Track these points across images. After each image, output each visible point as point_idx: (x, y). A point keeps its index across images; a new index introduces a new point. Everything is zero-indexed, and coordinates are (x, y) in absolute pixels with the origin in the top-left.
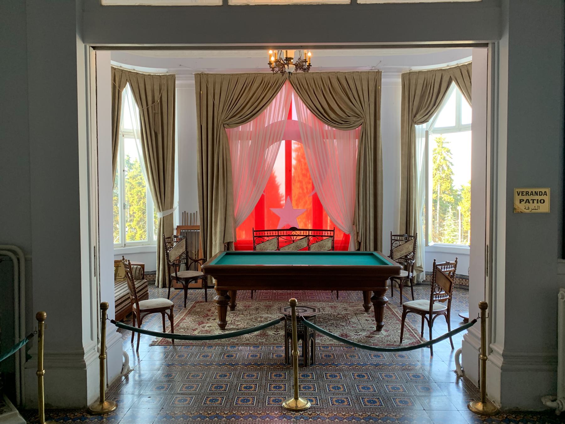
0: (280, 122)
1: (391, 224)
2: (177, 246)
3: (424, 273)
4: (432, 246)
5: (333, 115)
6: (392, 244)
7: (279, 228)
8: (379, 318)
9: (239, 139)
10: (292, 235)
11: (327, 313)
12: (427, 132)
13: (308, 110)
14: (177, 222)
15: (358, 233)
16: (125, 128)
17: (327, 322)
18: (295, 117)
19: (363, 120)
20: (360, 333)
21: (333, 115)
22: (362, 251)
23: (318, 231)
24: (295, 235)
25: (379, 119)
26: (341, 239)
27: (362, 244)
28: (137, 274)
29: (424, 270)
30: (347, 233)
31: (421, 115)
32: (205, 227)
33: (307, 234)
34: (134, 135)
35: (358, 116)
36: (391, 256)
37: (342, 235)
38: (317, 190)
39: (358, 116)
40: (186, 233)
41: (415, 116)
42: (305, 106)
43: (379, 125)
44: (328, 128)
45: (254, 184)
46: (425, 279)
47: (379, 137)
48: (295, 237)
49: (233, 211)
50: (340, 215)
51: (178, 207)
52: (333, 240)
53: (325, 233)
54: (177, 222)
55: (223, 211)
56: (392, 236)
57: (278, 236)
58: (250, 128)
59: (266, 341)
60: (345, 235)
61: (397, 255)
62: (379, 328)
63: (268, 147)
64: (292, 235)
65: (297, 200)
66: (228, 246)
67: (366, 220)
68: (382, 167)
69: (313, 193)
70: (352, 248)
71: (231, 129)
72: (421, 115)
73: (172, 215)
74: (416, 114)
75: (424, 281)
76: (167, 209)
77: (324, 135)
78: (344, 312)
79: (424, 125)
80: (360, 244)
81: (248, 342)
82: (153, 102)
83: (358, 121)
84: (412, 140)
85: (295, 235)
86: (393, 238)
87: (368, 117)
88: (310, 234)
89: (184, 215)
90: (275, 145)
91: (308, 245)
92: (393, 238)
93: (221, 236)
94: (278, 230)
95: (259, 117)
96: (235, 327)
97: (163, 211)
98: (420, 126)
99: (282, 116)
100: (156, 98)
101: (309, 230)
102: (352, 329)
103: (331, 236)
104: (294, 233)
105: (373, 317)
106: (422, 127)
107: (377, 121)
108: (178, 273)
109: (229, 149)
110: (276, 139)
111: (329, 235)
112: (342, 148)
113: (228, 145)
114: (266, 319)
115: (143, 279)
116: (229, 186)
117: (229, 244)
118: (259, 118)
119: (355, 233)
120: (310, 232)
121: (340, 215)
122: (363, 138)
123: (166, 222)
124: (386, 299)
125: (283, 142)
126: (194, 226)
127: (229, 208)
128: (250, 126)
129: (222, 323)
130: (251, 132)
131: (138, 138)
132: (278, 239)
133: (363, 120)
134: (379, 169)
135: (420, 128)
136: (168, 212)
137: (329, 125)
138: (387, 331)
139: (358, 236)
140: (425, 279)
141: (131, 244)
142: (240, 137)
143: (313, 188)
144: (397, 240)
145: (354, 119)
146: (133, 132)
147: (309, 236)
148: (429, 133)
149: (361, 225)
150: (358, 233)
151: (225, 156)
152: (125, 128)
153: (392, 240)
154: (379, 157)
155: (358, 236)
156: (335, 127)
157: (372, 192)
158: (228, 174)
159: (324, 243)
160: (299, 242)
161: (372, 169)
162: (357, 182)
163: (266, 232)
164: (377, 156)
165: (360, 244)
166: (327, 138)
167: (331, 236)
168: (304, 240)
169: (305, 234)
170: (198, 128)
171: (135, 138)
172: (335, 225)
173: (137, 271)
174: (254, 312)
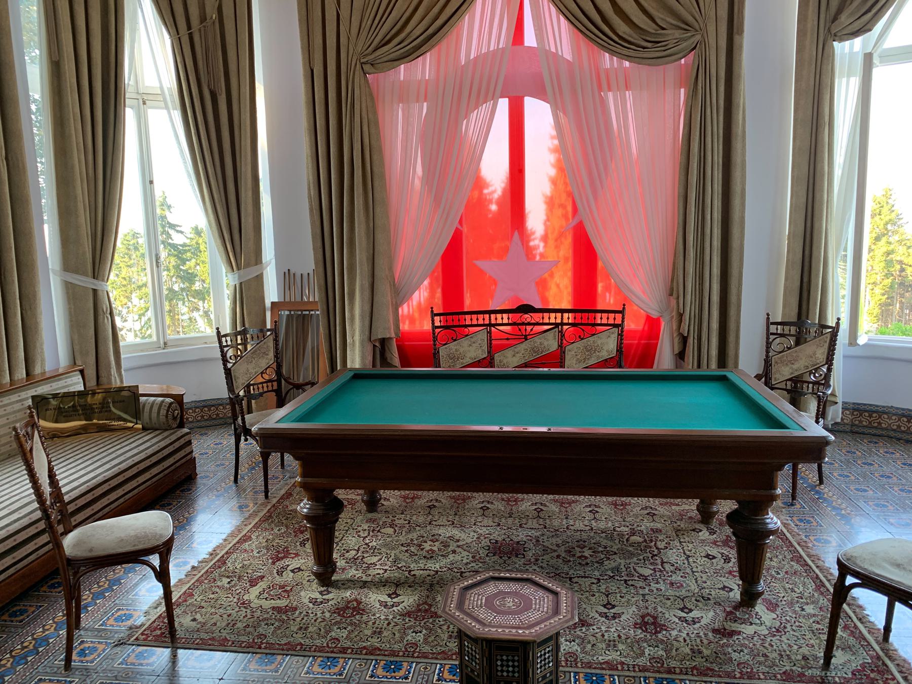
0: (495, 52)
1: (761, 295)
2: (254, 351)
3: (840, 405)
4: (865, 345)
5: (623, 28)
6: (768, 345)
7: (492, 307)
8: (750, 569)
9: (401, 100)
10: (523, 324)
11: (602, 525)
12: (868, 59)
13: (562, 18)
14: (272, 293)
15: (681, 316)
16: (146, 84)
17: (601, 562)
18: (530, 39)
19: (698, 37)
20: (695, 614)
21: (623, 28)
22: (689, 368)
23: (585, 315)
24: (529, 324)
25: (741, 31)
26: (640, 328)
27: (690, 340)
28: (162, 418)
29: (840, 400)
30: (655, 314)
31: (852, 14)
32: (331, 305)
33: (559, 321)
34: (165, 100)
35: (686, 26)
36: (765, 376)
37: (643, 321)
38: (583, 214)
39: (686, 26)
40: (296, 318)
41: (835, 19)
42: (553, 9)
43: (741, 46)
44: (611, 60)
45: (437, 200)
46: (839, 420)
47: (739, 76)
48: (529, 328)
49: (391, 269)
50: (637, 278)
51: (274, 261)
52: (620, 335)
53: (599, 318)
54: (272, 293)
55: (366, 268)
56: (769, 323)
57: (490, 325)
58: (423, 72)
59: (426, 640)
60: (649, 318)
61: (782, 373)
62: (750, 597)
63: (467, 116)
64: (523, 324)
65: (556, 240)
66: (380, 348)
67: (702, 284)
68: (744, 155)
69: (575, 222)
70: (665, 359)
71: (381, 75)
72: (852, 14)
73: (259, 279)
74: (839, 11)
75: (836, 423)
76: (247, 265)
77: (603, 82)
78: (646, 525)
79: (857, 43)
80: (684, 340)
81: (375, 642)
82: (203, 18)
83: (685, 40)
84: (826, 80)
85: (529, 324)
86: (773, 329)
87: (711, 28)
88: (565, 321)
89: (287, 278)
90: (485, 108)
91: (561, 346)
92: (773, 329)
93: (363, 326)
94: (490, 312)
95: (444, 43)
96: (359, 574)
97: (239, 269)
98: (847, 43)
99: (500, 38)
100: (208, 10)
101: (562, 311)
102: (670, 592)
103: (615, 326)
104: (527, 317)
105: (726, 543)
106: (852, 47)
107: (736, 38)
108: (247, 417)
109: (377, 123)
110: (488, 95)
111: (611, 321)
112: (645, 113)
113: (375, 113)
114: (446, 546)
115: (181, 425)
116: (378, 210)
117: (384, 342)
118: (445, 45)
119: (674, 313)
120: (566, 315)
121: (637, 278)
122: (697, 83)
123: (248, 294)
124: (773, 520)
125: (503, 105)
126: (309, 302)
127: (380, 262)
128: (424, 68)
129: (321, 570)
130: (427, 81)
131: (174, 109)
132: (489, 333)
133: (698, 37)
134: (737, 158)
135: (847, 50)
136: (252, 272)
137: (613, 53)
138: (772, 607)
139: (680, 321)
140: (839, 420)
141: (179, 343)
142: (403, 95)
143: (575, 210)
144: (782, 335)
145: (678, 34)
146: (163, 93)
147: (562, 324)
148: (876, 60)
149: (688, 297)
150: (681, 316)
151: (366, 141)
152: (146, 84)
153: (768, 334)
154: (737, 130)
155: (680, 321)
156: (628, 57)
157: (717, 215)
158: (376, 184)
159: (599, 342)
160: (538, 340)
161: (719, 159)
162: (682, 191)
163: (468, 317)
164: (734, 126)
165: (684, 340)
166: (610, 89)
167: (615, 326)
168: (550, 335)
169: (552, 321)
170: (305, 76)
171: (167, 108)
172: (626, 298)
173: (163, 412)
174: (421, 519)
